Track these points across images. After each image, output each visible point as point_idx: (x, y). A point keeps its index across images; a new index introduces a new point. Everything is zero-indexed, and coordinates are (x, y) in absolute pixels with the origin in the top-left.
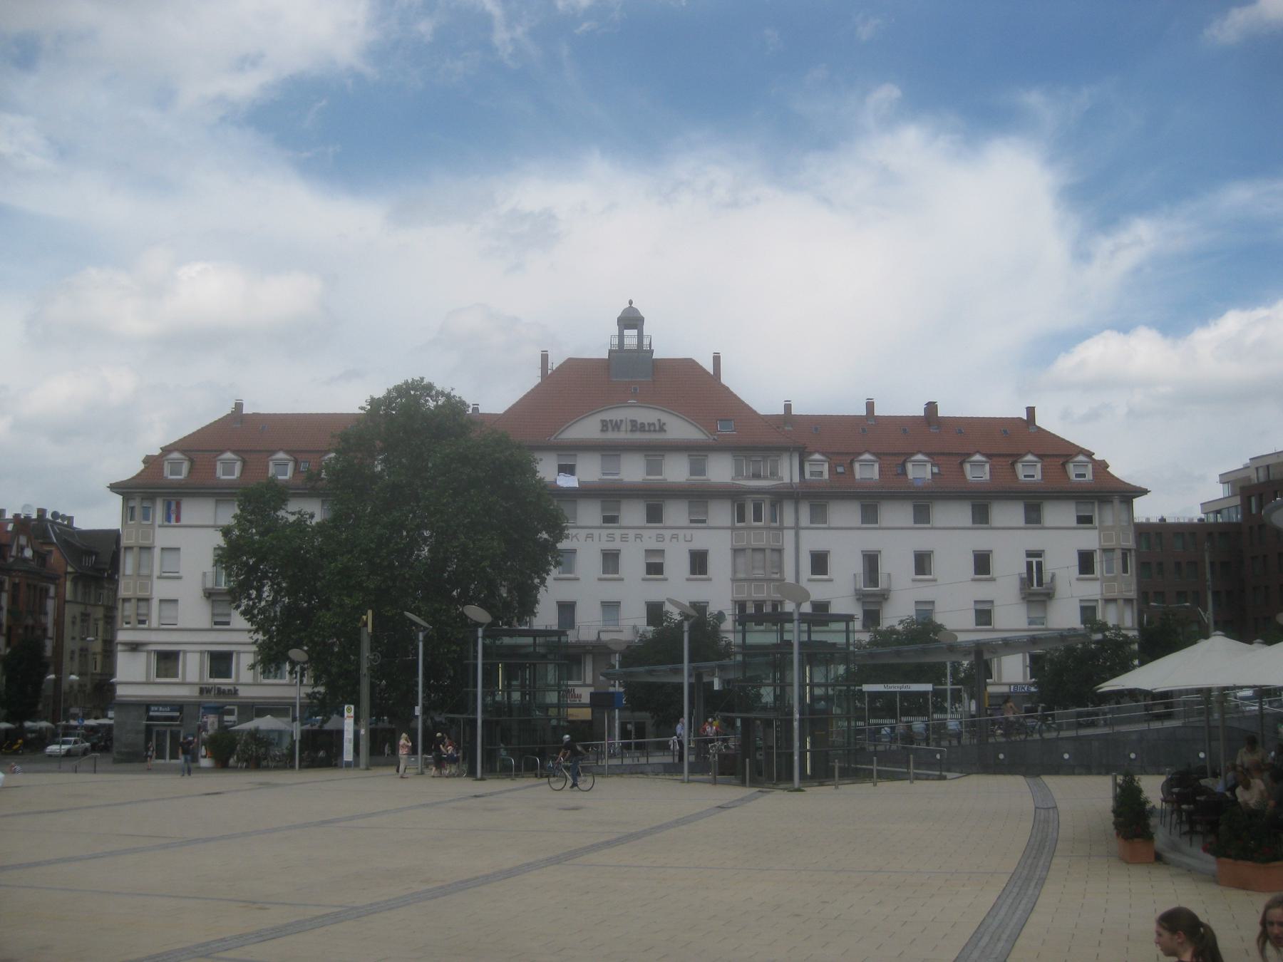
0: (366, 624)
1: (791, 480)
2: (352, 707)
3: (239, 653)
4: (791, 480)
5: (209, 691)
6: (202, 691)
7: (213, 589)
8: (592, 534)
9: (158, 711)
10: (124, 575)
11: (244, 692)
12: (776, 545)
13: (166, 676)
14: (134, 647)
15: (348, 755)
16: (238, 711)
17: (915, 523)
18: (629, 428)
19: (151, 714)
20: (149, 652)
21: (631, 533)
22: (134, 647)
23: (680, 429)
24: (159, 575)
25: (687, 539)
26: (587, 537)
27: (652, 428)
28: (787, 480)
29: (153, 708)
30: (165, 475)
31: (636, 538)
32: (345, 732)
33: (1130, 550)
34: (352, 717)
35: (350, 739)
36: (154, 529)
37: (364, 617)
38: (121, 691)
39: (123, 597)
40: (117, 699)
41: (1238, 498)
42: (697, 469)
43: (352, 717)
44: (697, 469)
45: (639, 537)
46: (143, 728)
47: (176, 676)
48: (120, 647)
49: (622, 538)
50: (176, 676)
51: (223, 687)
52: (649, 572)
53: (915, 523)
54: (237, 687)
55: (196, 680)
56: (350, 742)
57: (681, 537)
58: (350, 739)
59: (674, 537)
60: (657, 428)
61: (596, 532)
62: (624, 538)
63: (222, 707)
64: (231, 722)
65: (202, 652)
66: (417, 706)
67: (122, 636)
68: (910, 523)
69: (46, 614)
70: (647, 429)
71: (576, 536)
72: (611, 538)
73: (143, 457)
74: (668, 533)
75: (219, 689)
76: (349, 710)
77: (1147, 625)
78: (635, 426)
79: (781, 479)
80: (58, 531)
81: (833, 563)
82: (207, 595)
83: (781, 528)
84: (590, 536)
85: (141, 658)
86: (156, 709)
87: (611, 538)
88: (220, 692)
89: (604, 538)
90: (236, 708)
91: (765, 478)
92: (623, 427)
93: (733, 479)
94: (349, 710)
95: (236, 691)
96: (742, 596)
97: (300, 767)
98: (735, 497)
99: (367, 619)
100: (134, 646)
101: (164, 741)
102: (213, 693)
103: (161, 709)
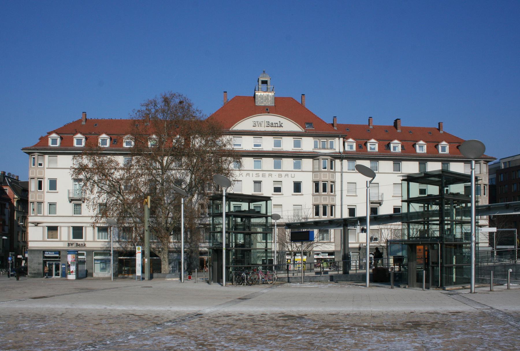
0: (147, 203)
1: (339, 150)
2: (140, 247)
3: (61, 227)
4: (339, 150)
5: (72, 244)
6: (69, 244)
7: (73, 198)
8: (249, 174)
9: (48, 254)
10: (31, 191)
11: (89, 246)
12: (332, 180)
13: (52, 238)
14: (37, 224)
15: (139, 273)
16: (86, 254)
17: (394, 171)
18: (266, 125)
19: (45, 255)
20: (43, 227)
21: (267, 173)
22: (37, 224)
23: (290, 126)
24: (47, 191)
25: (292, 176)
26: (285, 176)
27: (276, 125)
28: (337, 151)
29: (46, 253)
30: (49, 145)
31: (269, 175)
32: (137, 261)
33: (486, 185)
34: (140, 253)
35: (139, 264)
36: (44, 170)
37: (146, 200)
38: (31, 245)
39: (31, 201)
40: (29, 248)
41: (495, 175)
42: (297, 144)
43: (140, 253)
44: (297, 144)
45: (270, 175)
46: (42, 262)
47: (57, 238)
48: (30, 224)
49: (263, 175)
50: (57, 238)
51: (79, 243)
52: (275, 191)
53: (394, 171)
54: (85, 243)
55: (67, 240)
56: (139, 266)
57: (290, 176)
58: (139, 264)
59: (287, 175)
60: (279, 125)
61: (251, 173)
62: (263, 175)
63: (77, 251)
64: (82, 259)
65: (69, 227)
66: (255, 210)
67: (30, 219)
68: (392, 171)
69: (5, 215)
70: (274, 125)
71: (241, 174)
72: (258, 175)
73: (40, 137)
74: (283, 174)
75: (77, 244)
76: (139, 249)
77: (493, 218)
78: (269, 124)
79: (335, 149)
80: (10, 181)
81: (303, 187)
82: (70, 200)
83: (335, 172)
84: (248, 175)
85: (39, 229)
86: (47, 253)
87: (258, 175)
88: (78, 245)
89: (255, 175)
90: (85, 252)
91: (327, 149)
92: (263, 125)
93: (313, 149)
94: (139, 249)
95: (85, 245)
96: (317, 203)
97: (150, 259)
98: (313, 156)
99: (147, 200)
100: (36, 224)
101: (52, 268)
102: (74, 245)
103: (50, 253)
